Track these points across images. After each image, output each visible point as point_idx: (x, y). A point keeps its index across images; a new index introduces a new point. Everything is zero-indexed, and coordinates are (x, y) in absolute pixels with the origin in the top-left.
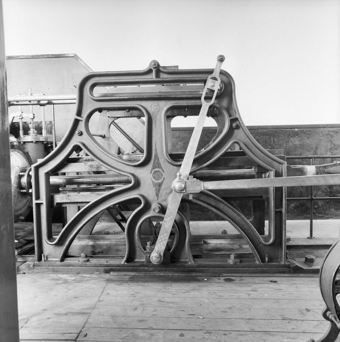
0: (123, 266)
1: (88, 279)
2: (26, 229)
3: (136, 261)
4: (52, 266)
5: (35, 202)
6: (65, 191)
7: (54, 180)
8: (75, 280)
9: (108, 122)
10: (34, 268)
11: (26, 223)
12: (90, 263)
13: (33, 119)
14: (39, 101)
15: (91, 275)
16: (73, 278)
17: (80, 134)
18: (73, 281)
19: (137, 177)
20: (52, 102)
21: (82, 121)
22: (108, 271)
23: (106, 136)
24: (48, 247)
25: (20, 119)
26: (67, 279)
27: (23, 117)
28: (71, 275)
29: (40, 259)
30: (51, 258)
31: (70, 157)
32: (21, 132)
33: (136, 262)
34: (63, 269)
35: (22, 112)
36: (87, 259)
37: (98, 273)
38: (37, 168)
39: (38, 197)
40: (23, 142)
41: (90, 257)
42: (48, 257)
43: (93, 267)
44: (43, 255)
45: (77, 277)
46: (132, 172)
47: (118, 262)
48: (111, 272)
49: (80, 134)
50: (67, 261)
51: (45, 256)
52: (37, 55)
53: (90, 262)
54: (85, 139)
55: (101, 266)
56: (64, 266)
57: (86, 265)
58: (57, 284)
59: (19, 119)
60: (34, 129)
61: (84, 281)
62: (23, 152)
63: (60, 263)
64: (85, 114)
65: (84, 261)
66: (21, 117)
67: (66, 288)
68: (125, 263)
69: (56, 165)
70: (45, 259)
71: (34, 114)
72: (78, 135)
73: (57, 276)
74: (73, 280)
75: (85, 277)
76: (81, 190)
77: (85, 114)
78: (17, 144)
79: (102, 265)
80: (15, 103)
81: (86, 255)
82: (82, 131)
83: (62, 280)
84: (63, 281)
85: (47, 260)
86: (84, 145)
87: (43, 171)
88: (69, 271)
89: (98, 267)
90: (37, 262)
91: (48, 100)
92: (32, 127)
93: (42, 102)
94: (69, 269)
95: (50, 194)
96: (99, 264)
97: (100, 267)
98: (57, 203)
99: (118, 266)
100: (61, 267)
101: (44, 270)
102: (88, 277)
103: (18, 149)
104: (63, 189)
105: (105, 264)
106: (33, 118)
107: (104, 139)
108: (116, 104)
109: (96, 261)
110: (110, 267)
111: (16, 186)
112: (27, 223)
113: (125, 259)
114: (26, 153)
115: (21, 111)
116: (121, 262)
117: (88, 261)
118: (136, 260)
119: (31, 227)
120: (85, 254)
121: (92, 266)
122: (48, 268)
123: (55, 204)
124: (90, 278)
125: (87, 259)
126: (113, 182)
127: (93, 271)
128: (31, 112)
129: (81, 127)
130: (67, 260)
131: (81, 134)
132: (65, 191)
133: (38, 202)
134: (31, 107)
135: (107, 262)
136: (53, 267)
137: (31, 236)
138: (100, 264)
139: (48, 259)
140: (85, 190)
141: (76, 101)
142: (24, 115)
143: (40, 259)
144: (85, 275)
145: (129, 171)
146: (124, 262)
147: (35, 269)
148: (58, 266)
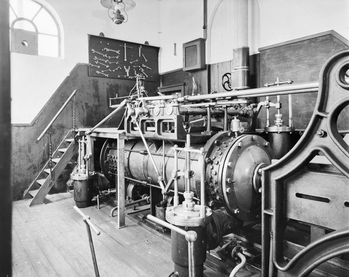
5: (264, 211)
21: (326, 117)
25: (267, 109)
38: (268, 173)
59: (267, 108)
64: (331, 108)
66: (268, 106)
77: (331, 108)
82: (326, 131)
129: (325, 125)
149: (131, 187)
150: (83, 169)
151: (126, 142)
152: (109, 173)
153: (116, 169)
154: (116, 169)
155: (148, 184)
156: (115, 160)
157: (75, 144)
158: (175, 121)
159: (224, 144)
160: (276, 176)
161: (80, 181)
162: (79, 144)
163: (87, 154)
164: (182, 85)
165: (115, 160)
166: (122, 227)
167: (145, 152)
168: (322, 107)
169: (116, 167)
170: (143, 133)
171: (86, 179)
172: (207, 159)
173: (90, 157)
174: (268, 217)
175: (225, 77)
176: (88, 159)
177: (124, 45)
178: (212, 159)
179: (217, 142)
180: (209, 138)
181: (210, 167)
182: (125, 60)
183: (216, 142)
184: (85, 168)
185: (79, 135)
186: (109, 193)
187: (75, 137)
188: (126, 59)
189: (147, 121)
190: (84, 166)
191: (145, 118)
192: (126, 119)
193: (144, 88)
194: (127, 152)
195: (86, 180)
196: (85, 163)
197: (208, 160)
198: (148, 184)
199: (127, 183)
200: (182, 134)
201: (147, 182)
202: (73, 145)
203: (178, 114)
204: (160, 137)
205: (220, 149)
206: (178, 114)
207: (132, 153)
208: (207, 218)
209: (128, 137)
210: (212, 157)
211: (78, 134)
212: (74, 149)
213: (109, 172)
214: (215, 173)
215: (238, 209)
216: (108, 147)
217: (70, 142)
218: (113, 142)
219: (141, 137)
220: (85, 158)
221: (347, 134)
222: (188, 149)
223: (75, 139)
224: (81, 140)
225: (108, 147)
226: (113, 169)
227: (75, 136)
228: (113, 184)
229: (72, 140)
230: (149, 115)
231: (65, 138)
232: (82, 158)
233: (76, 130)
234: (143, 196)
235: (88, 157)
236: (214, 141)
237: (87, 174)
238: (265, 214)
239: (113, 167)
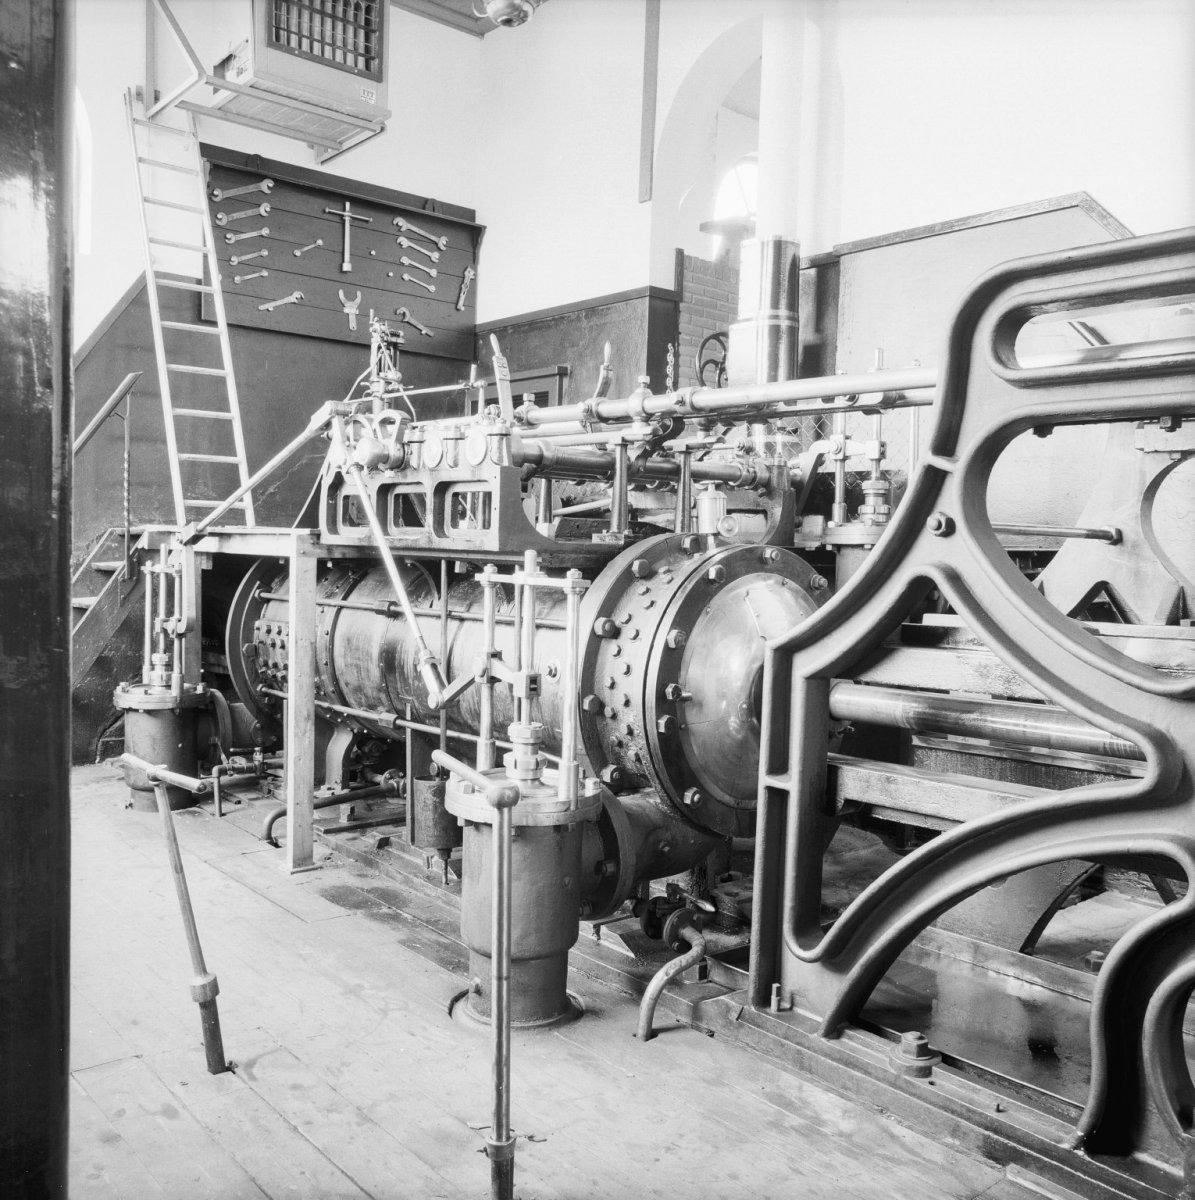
0: (1066, 1158)
1: (897, 1151)
2: (848, 855)
3: (1138, 1163)
4: (798, 1044)
5: (765, 780)
6: (931, 749)
7: (851, 700)
8: (848, 1136)
9: (1143, 473)
10: (741, 1026)
11: (860, 831)
12: (930, 1087)
13: (879, 460)
14: (853, 398)
15: (924, 1139)
16: (846, 1126)
17: (941, 531)
18: (836, 1139)
19: (1182, 753)
20: (902, 397)
22: (999, 1155)
23: (1125, 539)
24: (801, 967)
25: (839, 463)
26: (825, 1117)
27: (847, 454)
28: (850, 1105)
29: (763, 1000)
30: (806, 1009)
31: (1096, 600)
32: (838, 509)
33: (1140, 1170)
34: (831, 1068)
35: (847, 438)
36: (921, 1063)
37: (957, 1142)
39: (779, 766)
40: (834, 545)
41: (938, 1059)
42: (796, 1002)
43: (940, 1107)
44: (775, 986)
45: (866, 1125)
46: (1161, 724)
47: (1053, 1129)
48: (1012, 1166)
49: (941, 531)
50: (851, 1043)
51: (786, 995)
52: (943, 224)
53: (932, 1083)
54: (963, 553)
55: (969, 1115)
56: (834, 1059)
57: (914, 1091)
58: (776, 1125)
59: (836, 460)
60: (880, 499)
61: (876, 1160)
62: (801, 583)
63: (823, 1040)
64: (969, 441)
65: (909, 1070)
66: (840, 456)
67: (793, 1160)
68: (1076, 1147)
69: (845, 650)
70: (786, 1005)
71: (883, 445)
72: (940, 535)
73: (800, 1088)
74: (841, 1134)
75: (893, 1137)
76: (993, 757)
77: (969, 441)
78: (774, 555)
79: (977, 1118)
80: (782, 407)
81: (923, 1042)
83: (805, 1117)
84: (802, 1121)
85: (791, 1009)
86: (954, 578)
87: (806, 664)
88: (849, 1084)
89: (960, 1115)
90: (753, 1009)
91: (884, 391)
92: (871, 491)
93: (865, 400)
94: (851, 1078)
95: (822, 757)
96: (963, 1106)
97: (968, 1119)
98: (849, 802)
99: (1045, 1150)
100: (823, 1058)
101: (771, 1046)
102: (903, 1146)
103: (780, 572)
104: (925, 742)
105: (987, 1116)
106: (877, 456)
107: (1118, 547)
108: (1117, 394)
109: (960, 1087)
110: (1008, 1137)
111: (744, 706)
112: (863, 833)
113: (1080, 1134)
114: (817, 589)
115: (844, 432)
116: (1062, 1134)
117: (926, 1072)
118: (1142, 1157)
119: (870, 850)
120: (921, 1038)
121: (934, 1099)
122: (783, 1045)
123: (840, 804)
124: (911, 1151)
125: (921, 1063)
126: (1125, 750)
127: (936, 1126)
128: (874, 436)
129: (950, 502)
130: (850, 1038)
131: (949, 529)
132: (931, 749)
133: (778, 782)
134: (839, 419)
135: (998, 1110)
136: (798, 1047)
137: (847, 888)
138: (969, 1110)
139: (795, 1009)
140: (1006, 759)
141: (937, 395)
142: (852, 448)
143: (763, 1000)
144: (900, 1131)
145: (1145, 718)
146: (1073, 1142)
147: (742, 1031)
148: (815, 1051)
149: (340, 744)
150: (160, 671)
151: (322, 571)
152: (258, 689)
153: (284, 672)
154: (284, 672)
155: (399, 722)
156: (283, 642)
157: (130, 578)
158: (494, 487)
159: (665, 573)
160: (806, 664)
161: (149, 712)
162: (148, 579)
163: (177, 615)
164: (554, 375)
165: (283, 642)
166: (299, 869)
167: (393, 608)
168: (946, 443)
169: (286, 667)
170: (385, 532)
171: (170, 706)
172: (602, 620)
173: (189, 629)
174: (778, 797)
175: (712, 341)
176: (180, 636)
177: (344, 210)
178: (617, 623)
179: (641, 565)
180: (611, 554)
181: (610, 647)
182: (347, 267)
183: (635, 567)
184: (169, 666)
185: (146, 547)
186: (257, 763)
187: (131, 553)
188: (351, 261)
189: (399, 490)
190: (165, 658)
191: (388, 476)
192: (327, 482)
193: (399, 375)
194: (326, 608)
195: (172, 710)
196: (169, 648)
197: (605, 623)
198: (399, 722)
199: (325, 725)
200: (515, 527)
201: (396, 716)
202: (124, 581)
203: (506, 463)
204: (439, 543)
205: (648, 590)
206: (506, 463)
207: (344, 612)
208: (581, 801)
209: (330, 548)
210: (619, 619)
211: (143, 543)
212: (124, 598)
213: (261, 685)
214: (625, 670)
215: (695, 789)
216: (255, 592)
217: (109, 573)
218: (273, 570)
219: (375, 549)
220: (170, 626)
221: (1069, 540)
222: (531, 575)
223: (130, 558)
224: (153, 565)
225: (256, 595)
226: (274, 676)
227: (129, 549)
228: (272, 736)
229: (120, 565)
230: (401, 465)
231: (90, 557)
232: (158, 629)
233: (134, 530)
234: (386, 774)
235: (182, 628)
236: (631, 565)
237: (175, 692)
238: (770, 790)
239: (275, 666)
